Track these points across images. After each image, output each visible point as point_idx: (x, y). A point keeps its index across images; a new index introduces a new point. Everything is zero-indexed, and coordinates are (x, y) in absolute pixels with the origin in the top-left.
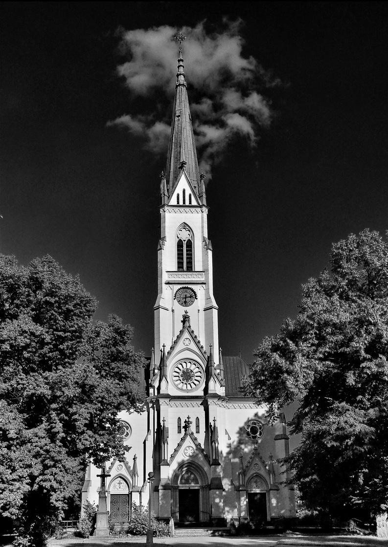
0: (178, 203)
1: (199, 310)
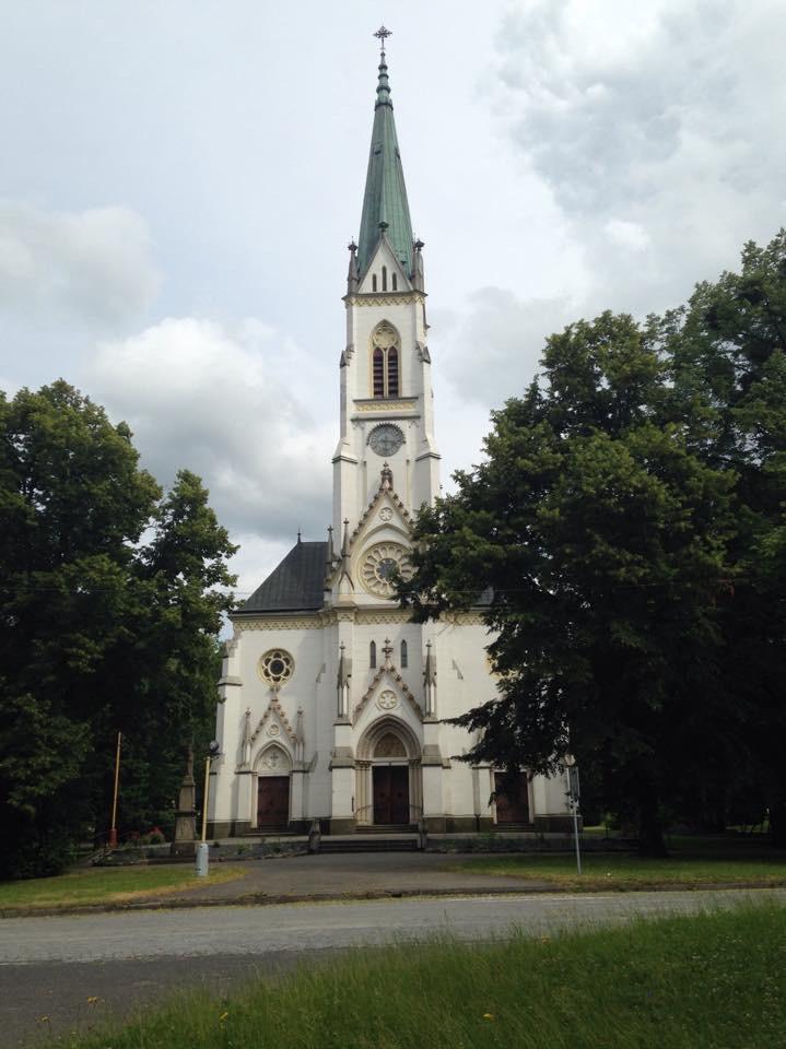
0: (375, 289)
1: (408, 461)
